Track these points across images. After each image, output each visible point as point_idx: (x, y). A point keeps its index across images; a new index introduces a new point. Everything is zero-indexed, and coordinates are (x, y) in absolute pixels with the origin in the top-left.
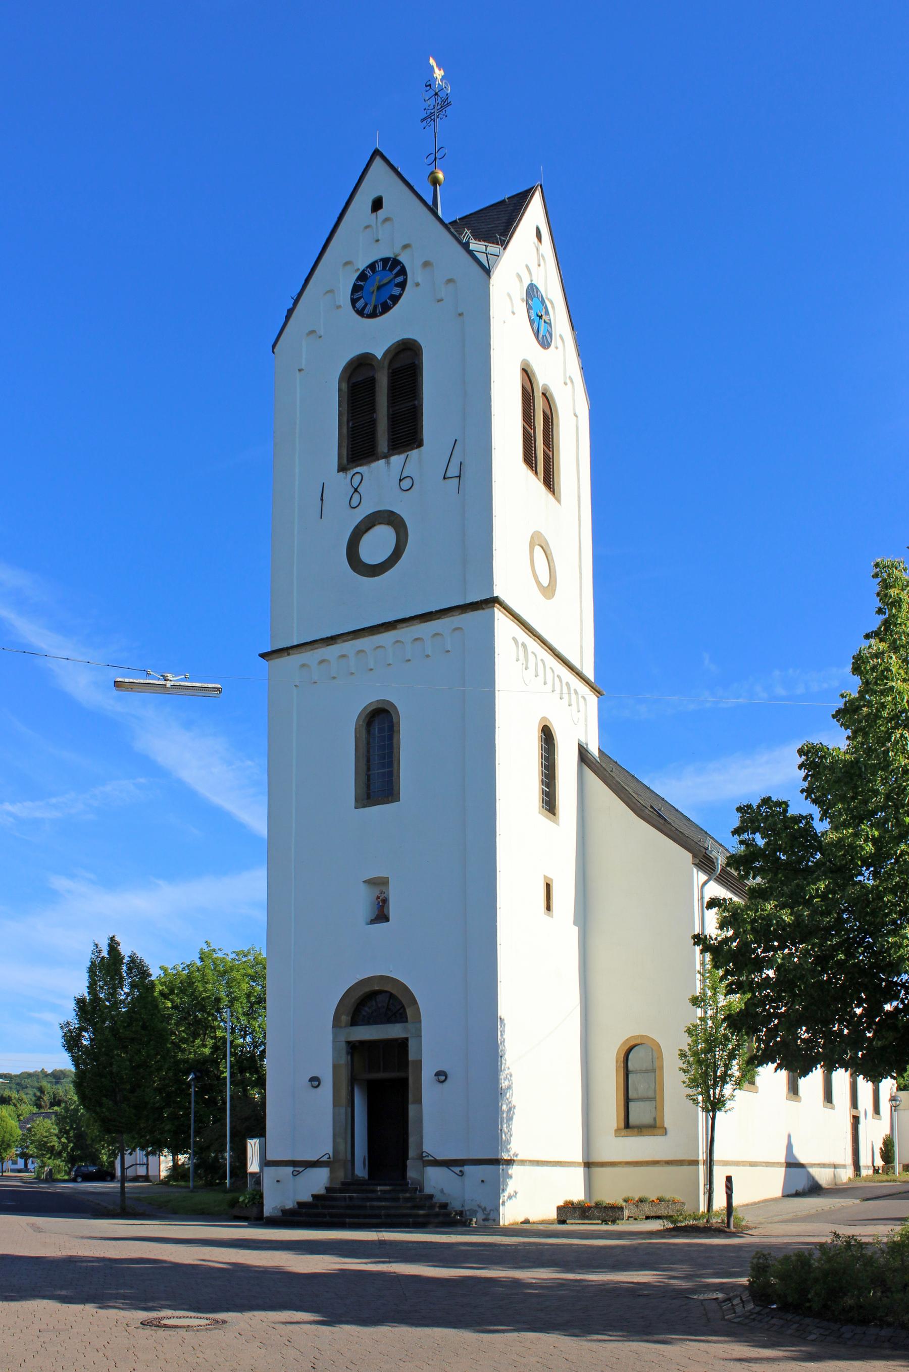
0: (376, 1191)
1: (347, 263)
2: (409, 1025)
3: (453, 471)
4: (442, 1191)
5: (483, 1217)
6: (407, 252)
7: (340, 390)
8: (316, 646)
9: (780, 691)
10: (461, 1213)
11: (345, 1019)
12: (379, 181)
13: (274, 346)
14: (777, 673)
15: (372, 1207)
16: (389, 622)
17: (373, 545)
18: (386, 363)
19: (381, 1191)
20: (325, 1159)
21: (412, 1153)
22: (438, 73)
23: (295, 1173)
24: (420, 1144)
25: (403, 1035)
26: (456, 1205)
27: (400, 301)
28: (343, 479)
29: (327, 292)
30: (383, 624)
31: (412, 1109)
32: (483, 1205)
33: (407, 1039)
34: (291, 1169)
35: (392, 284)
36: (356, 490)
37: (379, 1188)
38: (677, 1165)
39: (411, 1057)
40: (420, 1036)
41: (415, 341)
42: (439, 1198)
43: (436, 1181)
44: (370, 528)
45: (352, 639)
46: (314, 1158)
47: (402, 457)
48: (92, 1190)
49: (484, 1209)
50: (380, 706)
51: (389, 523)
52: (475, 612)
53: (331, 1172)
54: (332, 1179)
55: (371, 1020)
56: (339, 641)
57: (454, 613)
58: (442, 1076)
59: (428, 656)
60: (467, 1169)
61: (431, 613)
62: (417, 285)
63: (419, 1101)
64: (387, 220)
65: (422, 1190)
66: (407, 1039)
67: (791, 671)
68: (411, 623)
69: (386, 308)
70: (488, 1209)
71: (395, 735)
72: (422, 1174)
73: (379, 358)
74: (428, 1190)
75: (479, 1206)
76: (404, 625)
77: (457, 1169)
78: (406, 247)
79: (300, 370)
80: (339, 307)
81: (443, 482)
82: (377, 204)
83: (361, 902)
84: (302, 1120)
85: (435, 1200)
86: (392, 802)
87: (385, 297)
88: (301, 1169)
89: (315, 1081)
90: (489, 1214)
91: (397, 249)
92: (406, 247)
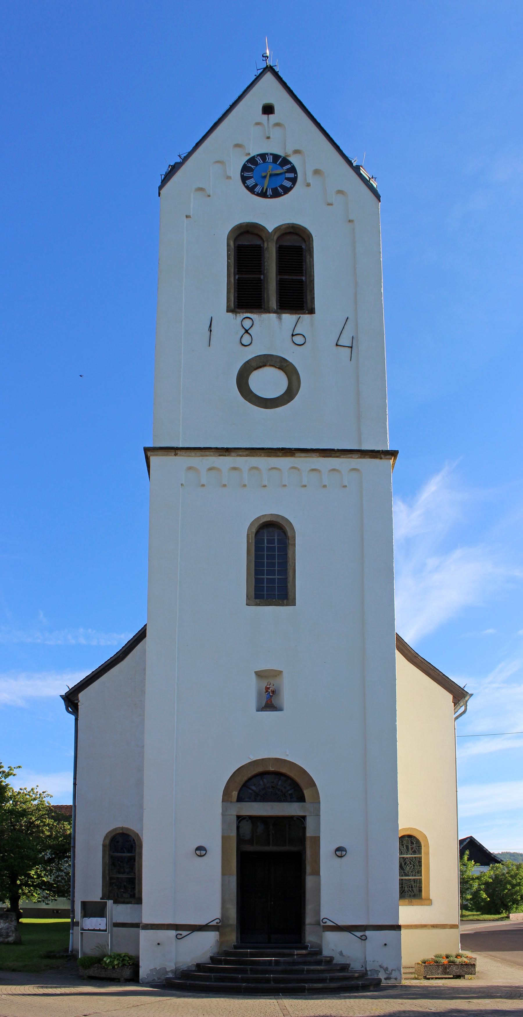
0: (293, 955)
1: (237, 146)
2: (307, 805)
3: (346, 341)
4: (341, 953)
5: (385, 976)
6: (298, 156)
7: (228, 245)
8: (208, 453)
9: (82, 641)
10: (364, 974)
11: (235, 794)
12: (268, 91)
13: (160, 188)
14: (81, 630)
15: (309, 971)
16: (290, 449)
17: (270, 384)
18: (275, 238)
19: (297, 955)
20: (214, 923)
21: (309, 919)
22: (268, 52)
23: (179, 937)
24: (318, 912)
25: (301, 814)
26: (356, 966)
27: (290, 193)
28: (235, 321)
29: (217, 162)
30: (283, 449)
31: (309, 881)
32: (385, 966)
33: (304, 817)
34: (173, 933)
35: (282, 177)
36: (247, 331)
37: (296, 952)
38: (441, 928)
39: (309, 833)
40: (318, 815)
41: (306, 229)
42: (338, 960)
43: (334, 945)
44: (260, 367)
45: (247, 456)
46: (202, 922)
47: (294, 317)
48: (418, 984)
49: (386, 969)
50: (274, 519)
51: (281, 368)
52: (373, 459)
53: (221, 935)
54: (221, 943)
55: (262, 797)
56: (233, 454)
57: (353, 456)
58: (340, 851)
59: (325, 486)
60: (368, 933)
61: (333, 450)
62: (308, 185)
63: (317, 872)
64: (277, 125)
65: (320, 952)
66: (304, 817)
67: (90, 630)
68: (309, 454)
69: (276, 194)
70: (390, 969)
71: (290, 547)
72: (321, 937)
73: (270, 231)
74: (326, 952)
75: (381, 967)
76: (303, 455)
77: (359, 934)
78: (296, 152)
79: (187, 217)
80: (229, 178)
81: (335, 348)
82: (268, 110)
83: (251, 690)
84: (189, 887)
85: (334, 962)
86: (287, 605)
87: (276, 182)
88: (184, 933)
89: (201, 851)
90: (391, 973)
91: (289, 150)
92: (296, 152)
